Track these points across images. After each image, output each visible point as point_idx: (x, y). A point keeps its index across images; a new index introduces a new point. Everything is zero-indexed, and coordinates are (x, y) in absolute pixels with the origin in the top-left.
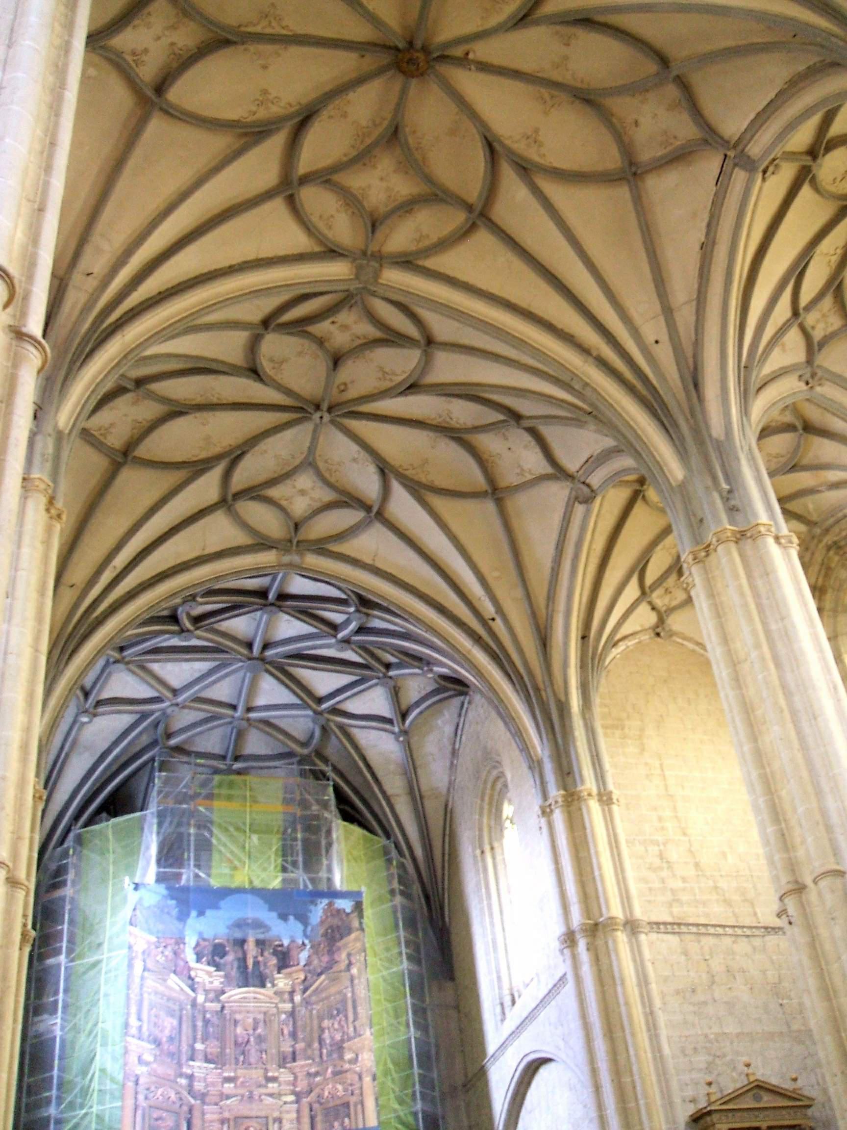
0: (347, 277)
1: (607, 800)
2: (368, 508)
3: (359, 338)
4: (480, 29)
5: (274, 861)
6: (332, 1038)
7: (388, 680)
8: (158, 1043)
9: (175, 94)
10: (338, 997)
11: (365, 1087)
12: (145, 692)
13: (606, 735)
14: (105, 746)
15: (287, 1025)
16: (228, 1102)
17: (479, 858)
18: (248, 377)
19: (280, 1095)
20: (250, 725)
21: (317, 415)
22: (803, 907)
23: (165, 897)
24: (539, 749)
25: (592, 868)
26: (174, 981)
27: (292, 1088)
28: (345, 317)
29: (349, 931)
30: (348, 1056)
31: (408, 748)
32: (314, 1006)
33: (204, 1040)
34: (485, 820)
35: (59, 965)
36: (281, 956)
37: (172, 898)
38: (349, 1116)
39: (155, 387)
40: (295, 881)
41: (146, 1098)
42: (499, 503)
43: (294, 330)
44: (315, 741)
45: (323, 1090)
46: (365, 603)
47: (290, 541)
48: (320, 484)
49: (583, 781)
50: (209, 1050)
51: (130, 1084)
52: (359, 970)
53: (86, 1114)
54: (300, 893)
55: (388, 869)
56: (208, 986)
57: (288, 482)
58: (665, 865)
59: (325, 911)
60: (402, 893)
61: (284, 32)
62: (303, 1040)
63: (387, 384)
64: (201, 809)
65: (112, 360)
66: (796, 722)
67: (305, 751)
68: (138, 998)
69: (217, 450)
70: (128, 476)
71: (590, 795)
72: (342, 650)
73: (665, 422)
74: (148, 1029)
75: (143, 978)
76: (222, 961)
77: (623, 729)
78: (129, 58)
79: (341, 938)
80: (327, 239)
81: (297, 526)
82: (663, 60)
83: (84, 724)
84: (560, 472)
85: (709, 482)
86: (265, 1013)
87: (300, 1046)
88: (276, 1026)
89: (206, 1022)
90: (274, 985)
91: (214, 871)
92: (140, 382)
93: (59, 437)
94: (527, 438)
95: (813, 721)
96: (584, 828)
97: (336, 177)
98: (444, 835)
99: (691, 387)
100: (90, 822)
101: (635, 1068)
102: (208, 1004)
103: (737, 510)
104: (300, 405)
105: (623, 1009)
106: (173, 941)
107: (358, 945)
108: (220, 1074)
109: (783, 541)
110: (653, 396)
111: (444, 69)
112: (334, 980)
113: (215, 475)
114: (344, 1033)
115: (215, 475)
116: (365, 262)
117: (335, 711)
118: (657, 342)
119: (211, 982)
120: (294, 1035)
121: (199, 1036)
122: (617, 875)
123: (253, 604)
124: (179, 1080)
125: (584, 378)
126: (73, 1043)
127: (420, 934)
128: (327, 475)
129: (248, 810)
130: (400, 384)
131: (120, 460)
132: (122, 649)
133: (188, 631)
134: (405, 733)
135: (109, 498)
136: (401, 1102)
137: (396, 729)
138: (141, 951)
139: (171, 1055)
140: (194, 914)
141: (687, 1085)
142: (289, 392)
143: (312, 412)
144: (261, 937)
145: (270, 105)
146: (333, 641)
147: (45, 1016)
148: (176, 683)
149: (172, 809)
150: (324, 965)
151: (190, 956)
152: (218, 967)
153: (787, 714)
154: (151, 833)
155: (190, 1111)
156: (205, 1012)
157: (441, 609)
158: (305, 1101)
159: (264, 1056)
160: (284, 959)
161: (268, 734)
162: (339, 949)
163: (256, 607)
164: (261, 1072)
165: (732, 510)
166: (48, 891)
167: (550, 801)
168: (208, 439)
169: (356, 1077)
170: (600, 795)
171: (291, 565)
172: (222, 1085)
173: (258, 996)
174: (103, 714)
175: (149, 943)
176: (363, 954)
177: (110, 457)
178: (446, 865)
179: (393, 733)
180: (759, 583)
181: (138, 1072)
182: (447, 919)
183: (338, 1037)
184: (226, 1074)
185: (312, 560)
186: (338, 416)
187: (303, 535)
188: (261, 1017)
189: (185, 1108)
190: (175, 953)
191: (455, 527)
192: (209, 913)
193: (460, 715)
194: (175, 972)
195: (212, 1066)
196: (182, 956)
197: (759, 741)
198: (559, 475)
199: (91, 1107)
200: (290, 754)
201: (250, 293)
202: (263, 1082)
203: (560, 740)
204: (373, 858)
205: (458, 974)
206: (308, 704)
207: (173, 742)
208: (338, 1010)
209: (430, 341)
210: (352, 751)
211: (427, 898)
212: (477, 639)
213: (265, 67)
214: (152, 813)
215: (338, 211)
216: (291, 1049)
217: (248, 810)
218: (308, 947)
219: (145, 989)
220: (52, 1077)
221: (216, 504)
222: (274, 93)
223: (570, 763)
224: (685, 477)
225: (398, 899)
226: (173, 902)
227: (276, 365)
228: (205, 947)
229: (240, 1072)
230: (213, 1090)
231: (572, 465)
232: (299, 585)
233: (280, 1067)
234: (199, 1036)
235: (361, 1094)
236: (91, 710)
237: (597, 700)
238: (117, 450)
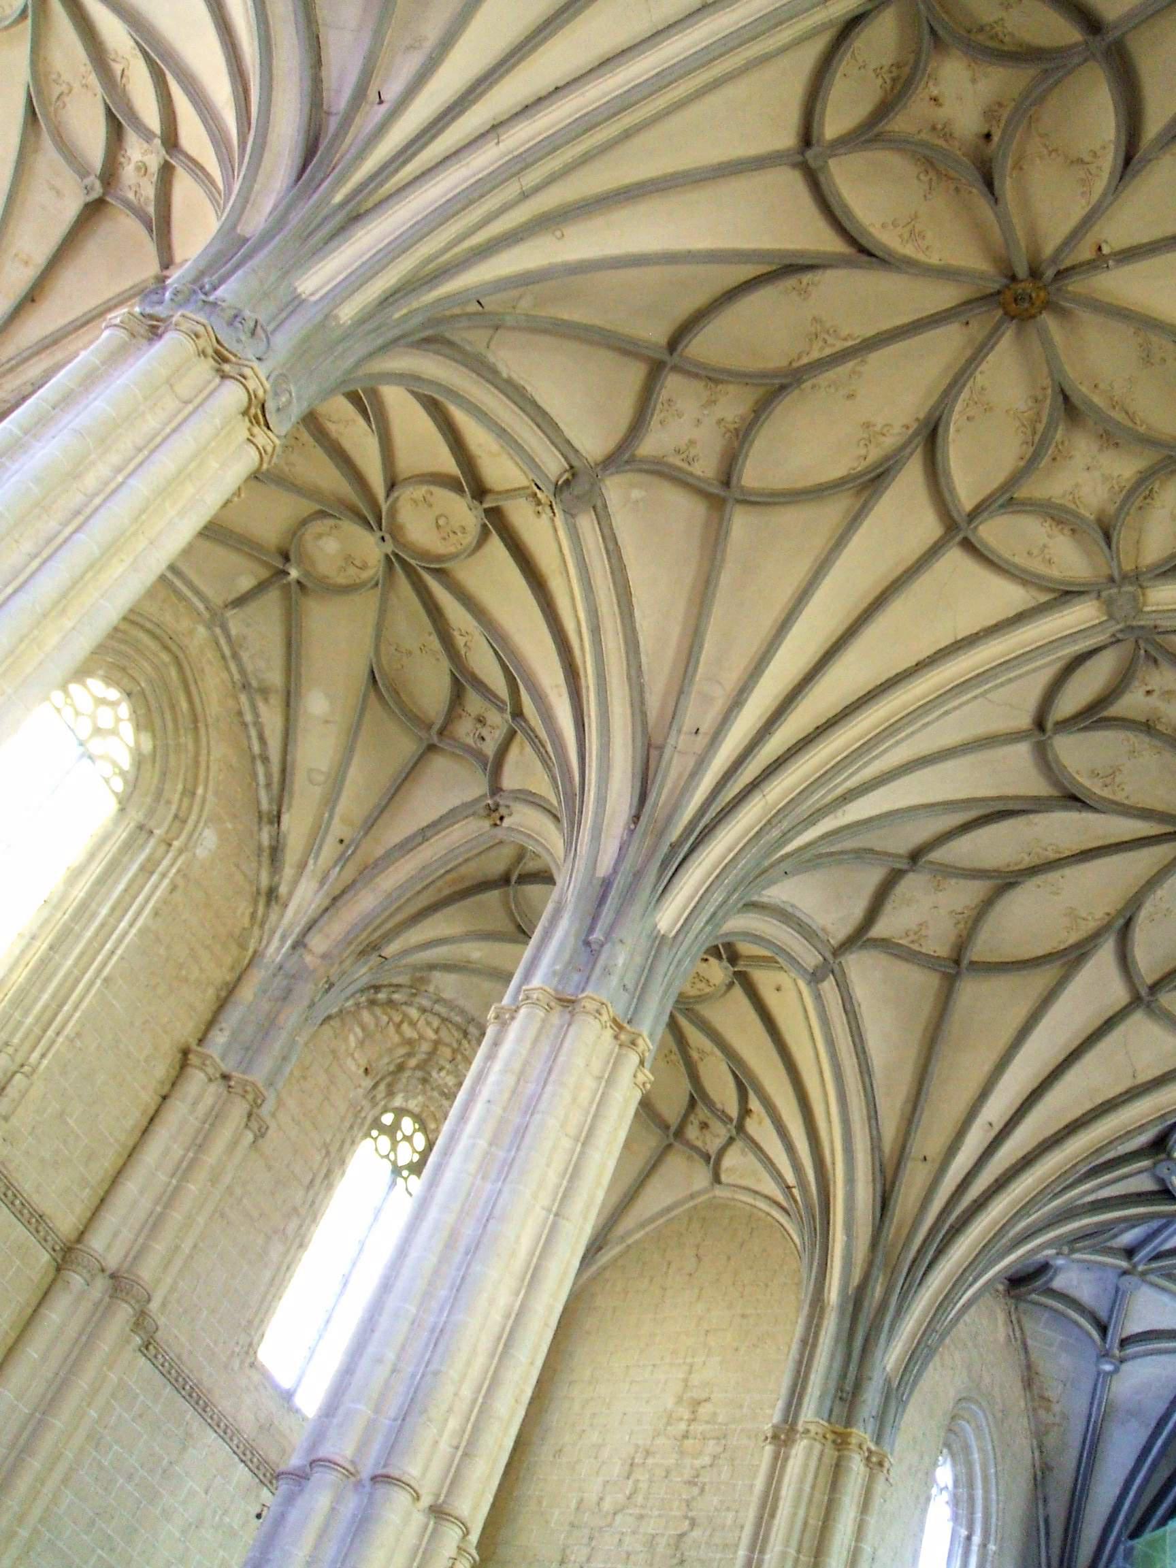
4: (1087, 209)
9: (752, 476)
18: (1065, 808)
39: (937, 855)
61: (850, 343)
69: (1091, 926)
70: (970, 991)
78: (676, 461)
80: (1051, 580)
84: (495, 768)
93: (659, 943)
97: (1022, 493)
111: (1075, 286)
142: (1146, 814)
145: (882, 439)
174: (1135, 1356)
213: (851, 396)
215: (1049, 536)
221: (1125, 1007)
222: (879, 422)
227: (1108, 780)
236: (1116, 1352)
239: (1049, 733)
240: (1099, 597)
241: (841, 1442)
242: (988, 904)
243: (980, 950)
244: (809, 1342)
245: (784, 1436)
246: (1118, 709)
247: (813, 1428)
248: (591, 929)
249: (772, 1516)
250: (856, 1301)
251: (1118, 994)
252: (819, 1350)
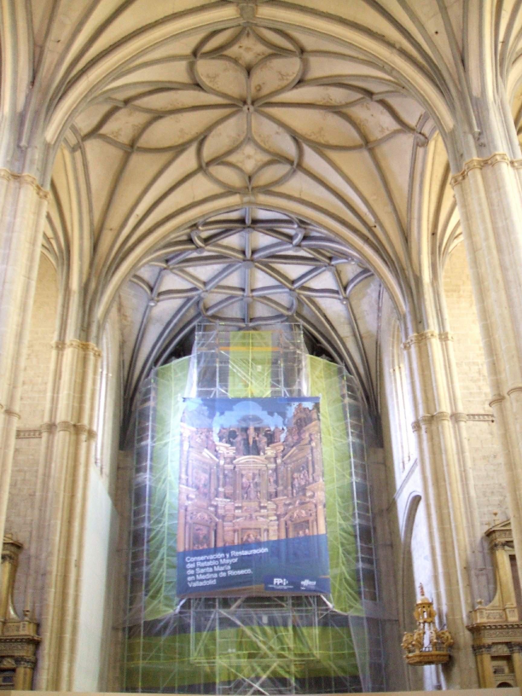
0: (235, 17)
1: (445, 338)
2: (291, 163)
3: (259, 55)
5: (268, 381)
6: (299, 484)
7: (332, 267)
8: (198, 488)
10: (304, 460)
11: (319, 511)
12: (186, 285)
13: (447, 296)
14: (168, 318)
15: (273, 477)
16: (238, 520)
17: (392, 374)
18: (195, 90)
19: (268, 516)
20: (254, 300)
21: (245, 108)
22: (502, 411)
23: (201, 405)
24: (404, 307)
25: (432, 382)
26: (207, 453)
27: (275, 512)
28: (246, 42)
29: (311, 420)
30: (309, 494)
31: (351, 309)
32: (289, 465)
33: (224, 485)
34: (395, 351)
35: (147, 445)
36: (269, 437)
37: (205, 405)
38: (308, 528)
39: (138, 102)
40: (280, 392)
41: (191, 518)
42: (371, 151)
43: (215, 56)
44: (294, 307)
45: (293, 513)
46: (302, 223)
47: (248, 188)
48: (259, 151)
49: (428, 327)
50: (227, 492)
51: (182, 511)
52: (316, 444)
53: (162, 527)
54: (281, 399)
55: (340, 382)
56: (226, 455)
57: (239, 151)
58: (482, 378)
59: (296, 409)
60: (350, 396)
62: (282, 484)
63: (285, 83)
64: (223, 352)
65: (81, 94)
66: (507, 288)
67: (290, 313)
68: (186, 463)
69: (187, 137)
70: (136, 159)
71: (432, 335)
72: (296, 251)
73: (441, 88)
74: (192, 481)
75: (188, 452)
76: (234, 441)
77: (459, 292)
79: (306, 425)
81: (250, 178)
83: (152, 307)
84: (405, 127)
85: (466, 128)
86: (259, 470)
87: (280, 488)
88: (266, 477)
89: (225, 476)
90: (265, 454)
91: (230, 389)
92: (127, 102)
93: (48, 147)
94: (380, 108)
95: (519, 288)
96: (428, 356)
99: (459, 62)
100: (166, 361)
101: (450, 504)
102: (226, 466)
103: (485, 146)
104: (233, 103)
105: (445, 468)
106: (206, 430)
107: (316, 428)
108: (233, 505)
109: (516, 164)
110: (435, 72)
112: (301, 450)
113: (192, 151)
114: (306, 480)
115: (192, 151)
116: (245, 4)
117: (303, 288)
118: (437, 33)
119: (228, 453)
120: (276, 482)
121: (221, 483)
122: (448, 385)
123: (238, 227)
124: (209, 508)
125: (391, 64)
126: (156, 488)
127: (362, 420)
128: (262, 144)
129: (250, 351)
130: (293, 80)
131: (129, 150)
132: (167, 261)
133: (201, 247)
134: (346, 298)
135: (127, 174)
136: (345, 519)
137: (341, 297)
138: (187, 436)
139: (205, 494)
140: (218, 414)
141: (484, 514)
142: (224, 95)
143: (241, 106)
144: (257, 426)
146: (291, 246)
147: (141, 474)
148: (204, 278)
149: (205, 354)
150: (295, 441)
151: (215, 438)
152: (232, 444)
153: (501, 283)
154: (193, 367)
155: (216, 525)
156: (224, 470)
157: (344, 223)
158: (282, 520)
159: (259, 494)
160: (271, 438)
161: (267, 305)
162: (304, 431)
163: (239, 229)
164: (257, 503)
165: (481, 146)
166: (141, 404)
167: (409, 340)
168: (182, 131)
169: (313, 506)
170: (440, 335)
171: (250, 203)
172: (234, 510)
173: (256, 460)
175: (192, 432)
176: (319, 434)
177: (123, 149)
178: (378, 378)
179: (339, 299)
180: (494, 195)
181: (186, 504)
182: (379, 411)
183: (303, 483)
184: (236, 505)
185: (262, 198)
186: (261, 106)
187: (256, 182)
188: (257, 472)
189: (213, 524)
190: (207, 437)
191: (345, 168)
192: (227, 413)
194: (207, 448)
195: (228, 500)
196: (211, 438)
197: (485, 303)
198: (404, 129)
199: (164, 523)
200: (281, 316)
201: (172, 36)
202: (258, 509)
203: (416, 302)
204: (330, 376)
205: (385, 444)
206: (285, 285)
207: (210, 313)
208: (303, 467)
209: (302, 51)
210: (317, 312)
211: (368, 398)
212: (366, 240)
214: (194, 357)
216: (274, 490)
217: (250, 351)
218: (286, 430)
219: (190, 458)
220: (145, 507)
223: (421, 316)
224: (454, 126)
225: (347, 400)
226: (206, 408)
228: (224, 433)
229: (245, 503)
230: (229, 514)
231: (412, 122)
232: (263, 215)
233: (268, 500)
234: (221, 483)
235: (316, 515)
237: (442, 274)
238: (126, 145)
239: (198, 58)
240: (237, 6)
241: (85, 347)
242: (149, 124)
243: (142, 142)
244: (66, 306)
245: (60, 346)
246: (230, 52)
247: (74, 343)
248: (19, 139)
249: (60, 378)
250: (85, 289)
251: (193, 164)
252: (70, 310)
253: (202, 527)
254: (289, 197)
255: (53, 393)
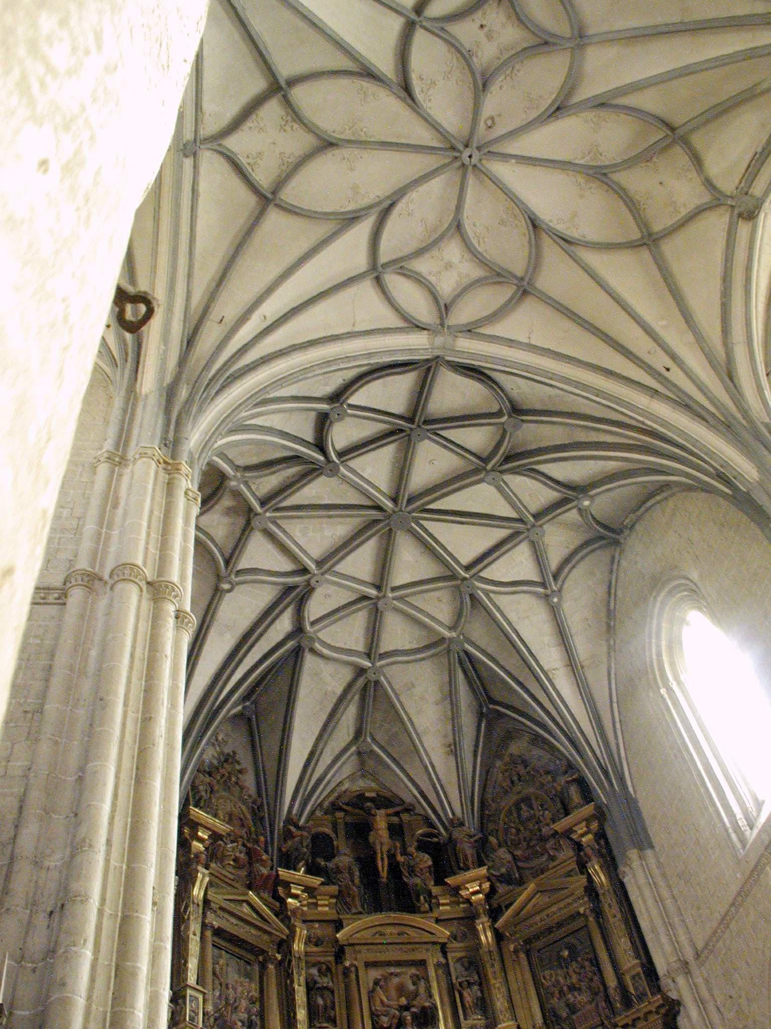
48: (467, 256)
70: (274, 218)
82: (673, 129)
98: (611, 702)
182: (631, 789)
193: (611, 572)
212: (654, 393)
253: (564, 759)
254: (511, 343)
255: (101, 525)
